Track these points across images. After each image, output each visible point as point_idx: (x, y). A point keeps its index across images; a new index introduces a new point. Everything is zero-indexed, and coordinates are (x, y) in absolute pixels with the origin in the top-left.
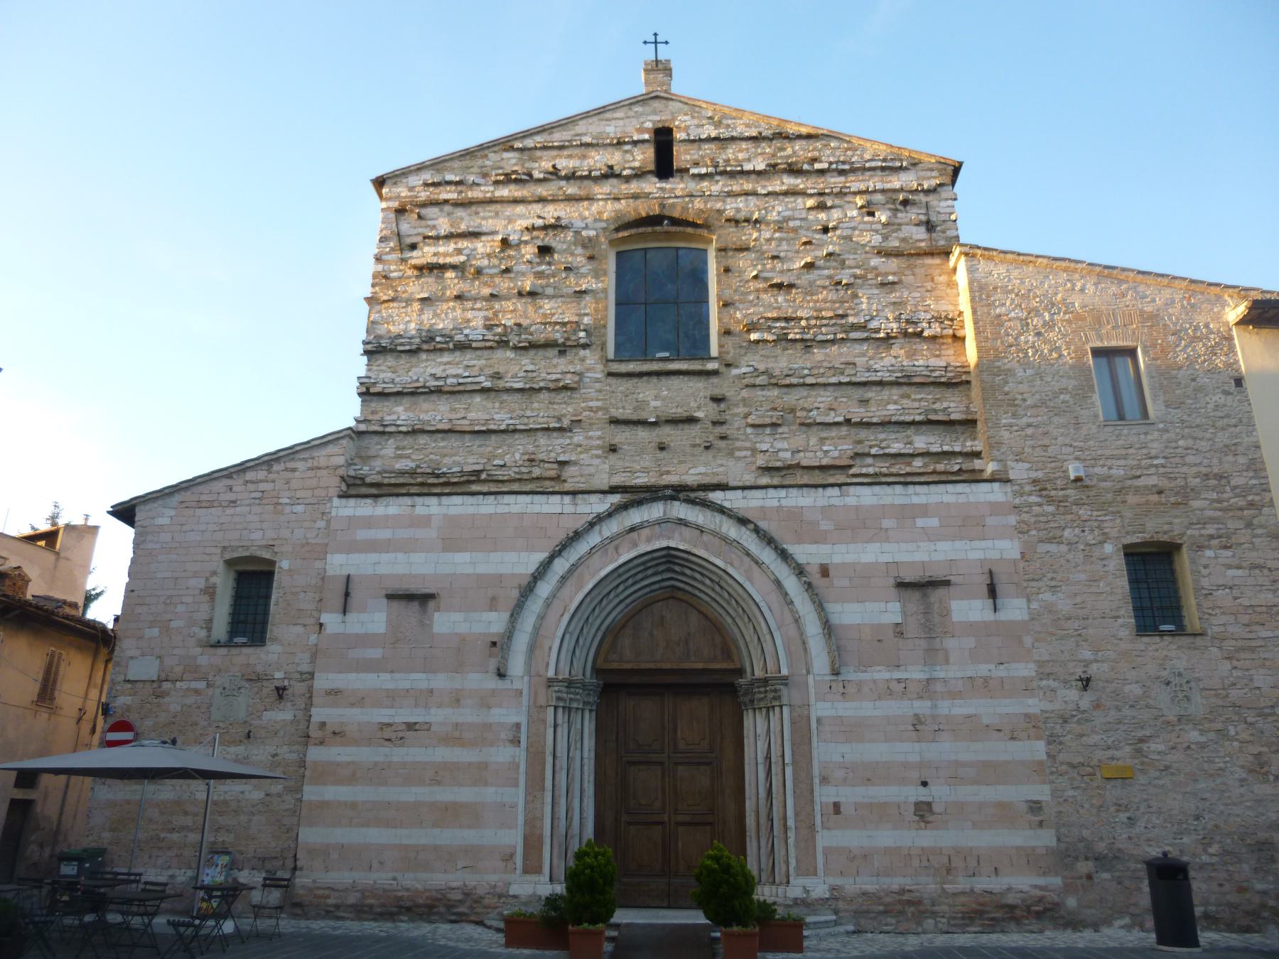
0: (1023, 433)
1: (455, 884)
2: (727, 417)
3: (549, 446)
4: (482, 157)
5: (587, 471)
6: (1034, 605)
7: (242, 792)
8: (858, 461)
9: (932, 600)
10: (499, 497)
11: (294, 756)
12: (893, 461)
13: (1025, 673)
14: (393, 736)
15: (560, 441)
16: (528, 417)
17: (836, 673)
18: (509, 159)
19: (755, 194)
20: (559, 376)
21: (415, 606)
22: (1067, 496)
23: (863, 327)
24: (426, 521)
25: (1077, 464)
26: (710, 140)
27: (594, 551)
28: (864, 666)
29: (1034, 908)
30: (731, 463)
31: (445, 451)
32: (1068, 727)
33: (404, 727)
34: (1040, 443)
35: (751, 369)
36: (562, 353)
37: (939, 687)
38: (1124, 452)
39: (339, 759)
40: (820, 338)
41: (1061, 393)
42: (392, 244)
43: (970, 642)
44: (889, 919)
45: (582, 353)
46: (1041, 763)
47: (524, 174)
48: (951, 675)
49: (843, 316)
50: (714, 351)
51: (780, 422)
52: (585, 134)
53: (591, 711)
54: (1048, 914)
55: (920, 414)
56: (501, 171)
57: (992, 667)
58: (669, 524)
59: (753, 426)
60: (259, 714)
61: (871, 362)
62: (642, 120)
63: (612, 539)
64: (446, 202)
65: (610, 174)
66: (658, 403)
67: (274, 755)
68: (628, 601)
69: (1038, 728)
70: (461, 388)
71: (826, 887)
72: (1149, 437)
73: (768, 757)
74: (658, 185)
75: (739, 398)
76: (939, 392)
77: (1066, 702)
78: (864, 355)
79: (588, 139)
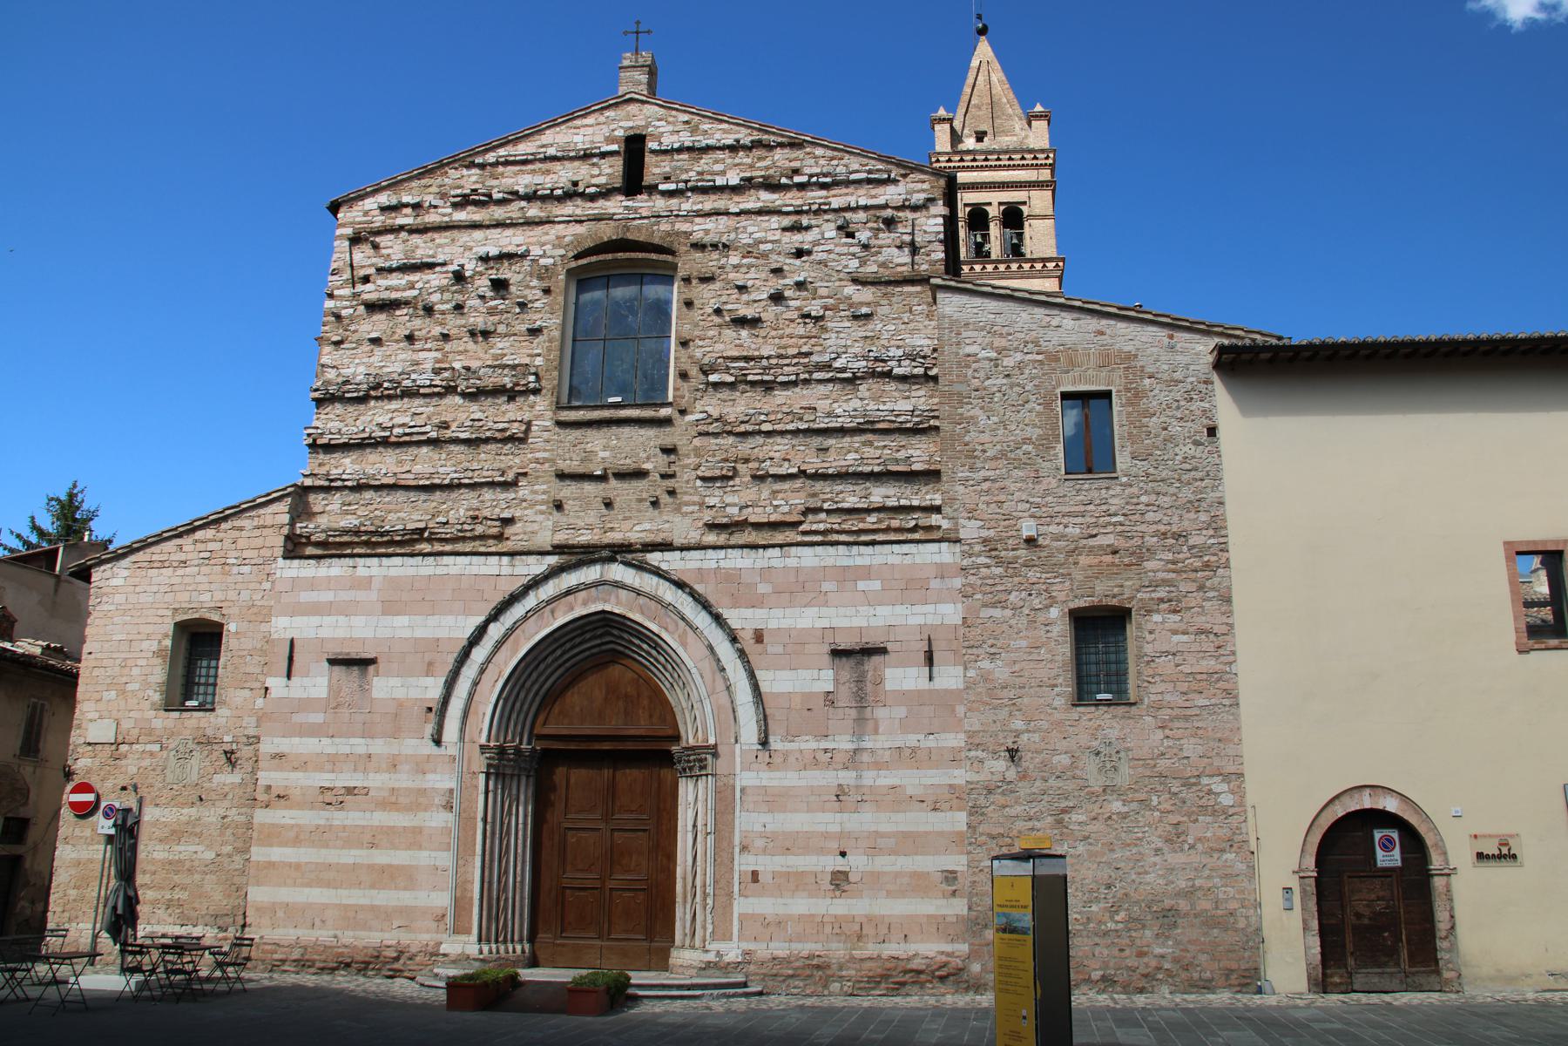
1: (389, 943)
2: (677, 469)
3: (494, 500)
6: (971, 673)
7: (196, 852)
8: (810, 517)
9: (866, 668)
11: (243, 818)
12: (848, 517)
14: (333, 800)
15: (504, 496)
16: (473, 470)
17: (764, 743)
18: (469, 176)
19: (727, 213)
20: (506, 425)
21: (355, 670)
22: (1018, 557)
23: (827, 367)
26: (680, 150)
27: (529, 615)
28: (791, 736)
29: (937, 973)
30: (677, 519)
31: (391, 507)
32: (992, 798)
33: (343, 791)
34: (995, 499)
36: (511, 399)
37: (865, 757)
38: (1082, 508)
39: (283, 821)
41: (1025, 443)
43: (901, 712)
45: (532, 398)
46: (959, 833)
47: (484, 195)
48: (879, 745)
50: (670, 399)
51: (730, 474)
52: (552, 145)
53: (528, 777)
54: (951, 978)
55: (879, 465)
56: (459, 191)
57: (921, 737)
58: (606, 587)
59: (703, 479)
60: (210, 777)
61: (835, 405)
63: (549, 602)
64: (402, 228)
66: (607, 454)
67: (223, 818)
68: (568, 665)
69: (961, 799)
70: (407, 438)
71: (740, 952)
72: (1111, 492)
74: (624, 204)
76: (902, 440)
77: (992, 773)
79: (551, 151)
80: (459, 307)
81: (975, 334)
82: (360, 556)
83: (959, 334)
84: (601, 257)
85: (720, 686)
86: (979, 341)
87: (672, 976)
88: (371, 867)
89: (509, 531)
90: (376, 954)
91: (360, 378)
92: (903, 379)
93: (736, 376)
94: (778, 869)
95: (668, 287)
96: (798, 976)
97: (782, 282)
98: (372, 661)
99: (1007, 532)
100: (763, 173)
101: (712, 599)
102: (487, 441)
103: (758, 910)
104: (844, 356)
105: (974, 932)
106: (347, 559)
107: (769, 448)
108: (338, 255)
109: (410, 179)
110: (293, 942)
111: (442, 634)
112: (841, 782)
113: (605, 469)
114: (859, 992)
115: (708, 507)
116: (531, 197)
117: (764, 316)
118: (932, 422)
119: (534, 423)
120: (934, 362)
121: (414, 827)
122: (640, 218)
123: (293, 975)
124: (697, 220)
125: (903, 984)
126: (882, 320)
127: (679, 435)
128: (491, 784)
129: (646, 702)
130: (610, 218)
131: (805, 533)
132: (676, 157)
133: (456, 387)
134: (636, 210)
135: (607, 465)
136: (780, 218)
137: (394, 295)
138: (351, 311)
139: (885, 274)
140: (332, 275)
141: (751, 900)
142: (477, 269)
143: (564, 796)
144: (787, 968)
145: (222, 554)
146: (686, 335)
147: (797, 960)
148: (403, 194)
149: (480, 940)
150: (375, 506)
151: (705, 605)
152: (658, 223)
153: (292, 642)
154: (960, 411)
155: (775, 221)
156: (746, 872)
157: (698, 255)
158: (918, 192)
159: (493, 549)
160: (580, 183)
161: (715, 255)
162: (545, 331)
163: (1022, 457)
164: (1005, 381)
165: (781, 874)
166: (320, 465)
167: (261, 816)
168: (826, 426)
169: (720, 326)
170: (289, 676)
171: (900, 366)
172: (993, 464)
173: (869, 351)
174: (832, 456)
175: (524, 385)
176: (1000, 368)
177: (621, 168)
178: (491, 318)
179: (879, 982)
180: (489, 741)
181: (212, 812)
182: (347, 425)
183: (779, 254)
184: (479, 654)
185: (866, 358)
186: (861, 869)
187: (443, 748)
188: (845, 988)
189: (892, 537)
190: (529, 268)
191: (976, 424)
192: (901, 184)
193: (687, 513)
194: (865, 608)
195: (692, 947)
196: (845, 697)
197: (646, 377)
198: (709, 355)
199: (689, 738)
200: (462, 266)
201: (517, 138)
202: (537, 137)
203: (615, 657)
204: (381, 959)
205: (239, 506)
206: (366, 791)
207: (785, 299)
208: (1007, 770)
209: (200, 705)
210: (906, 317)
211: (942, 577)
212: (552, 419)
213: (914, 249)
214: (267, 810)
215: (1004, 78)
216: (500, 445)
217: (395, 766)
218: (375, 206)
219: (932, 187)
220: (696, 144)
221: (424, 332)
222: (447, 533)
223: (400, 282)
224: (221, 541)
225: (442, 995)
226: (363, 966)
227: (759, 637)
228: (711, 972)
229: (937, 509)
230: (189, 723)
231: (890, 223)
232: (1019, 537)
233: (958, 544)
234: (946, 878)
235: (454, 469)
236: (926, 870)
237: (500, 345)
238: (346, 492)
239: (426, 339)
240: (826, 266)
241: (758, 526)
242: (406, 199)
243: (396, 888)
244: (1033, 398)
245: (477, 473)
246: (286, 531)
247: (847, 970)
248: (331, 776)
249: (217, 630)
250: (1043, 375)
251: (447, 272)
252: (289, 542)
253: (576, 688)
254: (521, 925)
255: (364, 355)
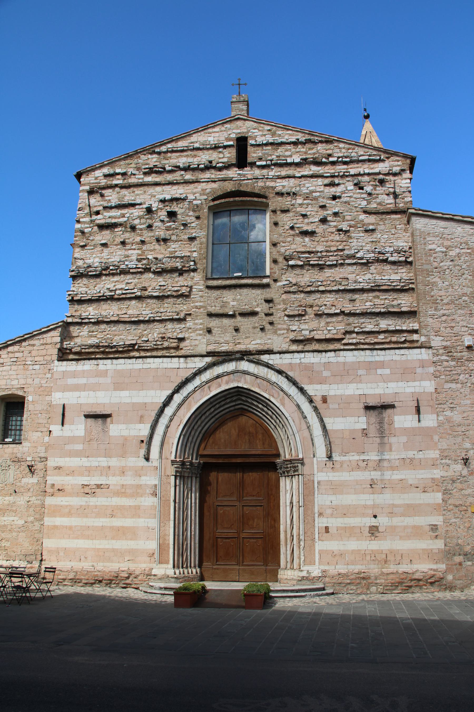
0: (440, 320)
1: (123, 569)
2: (274, 311)
3: (173, 328)
4: (137, 158)
5: (194, 343)
6: (441, 418)
7: (13, 521)
8: (348, 336)
9: (384, 415)
10: (145, 359)
11: (39, 502)
12: (368, 336)
13: (433, 456)
14: (89, 491)
15: (178, 326)
16: (161, 313)
17: (330, 457)
18: (152, 158)
19: (294, 177)
20: (179, 288)
21: (100, 421)
22: (463, 356)
23: (353, 257)
24: (105, 373)
25: (470, 337)
26: (266, 145)
27: (196, 389)
28: (344, 453)
29: (429, 581)
30: (275, 337)
31: (116, 333)
32: (455, 485)
33: (95, 487)
34: (449, 325)
35: (287, 282)
36: (181, 274)
37: (385, 464)
39: (62, 503)
40: (328, 263)
41: (463, 296)
42: (86, 212)
43: (404, 439)
44: (352, 587)
45: (192, 274)
46: (438, 505)
47: (161, 168)
48: (393, 457)
49: (342, 250)
50: (268, 273)
51: (303, 313)
52: (197, 142)
53: (196, 477)
54: (437, 583)
55: (384, 308)
56: (147, 166)
57: (415, 453)
58: (238, 374)
59: (288, 316)
60: (20, 479)
61: (358, 277)
62: (229, 133)
63: (207, 382)
64: (116, 185)
65: (209, 167)
66: (235, 303)
67: (28, 502)
68: (217, 417)
69: (438, 486)
70: (124, 296)
71: (320, 571)
73: (291, 503)
74: (238, 172)
75: (281, 299)
76: (395, 295)
77: (454, 471)
78: (353, 273)
79: (197, 145)
80: (150, 227)
81: (433, 239)
82: (100, 359)
83: (425, 239)
84: (227, 200)
85: (304, 426)
86: (436, 242)
87: (282, 584)
88: (112, 528)
89: (182, 345)
90: (116, 575)
91: (96, 265)
92: (394, 263)
93: (304, 262)
94: (340, 525)
95: (263, 216)
96: (353, 583)
97: (325, 212)
98: (109, 416)
99: (456, 343)
100: (312, 156)
101: (298, 380)
102: (168, 297)
103: (329, 548)
104: (362, 251)
105: (448, 558)
106: (93, 361)
107: (323, 299)
108: (82, 200)
109: (120, 160)
110: (69, 569)
111: (148, 400)
112: (373, 477)
113: (234, 311)
114: (387, 592)
115: (292, 331)
116: (187, 169)
117: (317, 230)
118: (411, 286)
119: (194, 287)
120: (410, 254)
121: (135, 506)
122: (247, 180)
123: (70, 587)
124: (278, 180)
125: (410, 587)
126: (381, 233)
127: (274, 293)
128: (178, 481)
129: (260, 436)
130: (231, 179)
131: (345, 344)
132: (264, 148)
133: (150, 268)
134: (244, 176)
135: (235, 309)
136: (323, 180)
137: (114, 221)
138: (90, 229)
139: (381, 208)
140: (79, 210)
141: (325, 542)
142: (159, 207)
143: (216, 488)
144: (346, 579)
145: (23, 359)
146: (275, 240)
147: (352, 575)
148: (116, 168)
149: (174, 567)
150: (107, 332)
151: (295, 383)
152: (257, 182)
153: (64, 405)
154: (428, 279)
155: (320, 181)
156: (322, 527)
157: (280, 199)
158: (396, 166)
159: (174, 354)
160: (213, 162)
161: (289, 199)
162: (198, 239)
163: (462, 303)
164: (451, 263)
165: (342, 528)
166: (76, 311)
167: (49, 501)
168: (354, 288)
169: (293, 235)
170: (63, 424)
171: (392, 256)
172: (447, 307)
173: (375, 248)
174: (357, 304)
175: (188, 267)
176: (448, 256)
177: (235, 154)
178: (168, 232)
179: (397, 586)
180: (176, 458)
181: (22, 499)
182: (90, 290)
183: (324, 198)
184: (169, 411)
185: (373, 252)
186: (385, 524)
187: (151, 462)
188: (379, 590)
189: (392, 346)
190: (188, 206)
191: (437, 286)
192: (387, 162)
193: (280, 334)
194: (382, 384)
195: (292, 569)
196: (373, 431)
197: (253, 263)
198: (289, 250)
199: (286, 454)
200: (151, 205)
201: (178, 139)
202: (188, 138)
203: (243, 412)
204: (119, 578)
205: (32, 333)
206: (108, 486)
207: (328, 221)
208: (463, 469)
209: (13, 440)
210: (393, 231)
211: (423, 367)
212: (204, 285)
213: (396, 196)
214: (53, 497)
215: (378, 140)
216: (175, 299)
217: (124, 472)
218: (101, 175)
219: (403, 164)
220: (275, 141)
221: (131, 240)
222: (148, 346)
223: (117, 214)
224: (23, 352)
225: (171, 599)
226: (109, 582)
227: (324, 400)
228: (304, 582)
229: (416, 332)
230: (7, 451)
231: (382, 182)
232: (463, 345)
233: (431, 349)
234: (432, 528)
235: (150, 312)
236: (421, 524)
237: (173, 246)
238: (91, 325)
239: (132, 244)
240: (349, 205)
241: (319, 341)
242: (118, 171)
243: (126, 539)
244: (467, 272)
245: (163, 314)
246: (58, 346)
247: (379, 580)
248: (89, 478)
249: (21, 401)
250: (471, 260)
251: (142, 208)
252: (60, 353)
253: (221, 429)
254: (194, 558)
255: (98, 253)
